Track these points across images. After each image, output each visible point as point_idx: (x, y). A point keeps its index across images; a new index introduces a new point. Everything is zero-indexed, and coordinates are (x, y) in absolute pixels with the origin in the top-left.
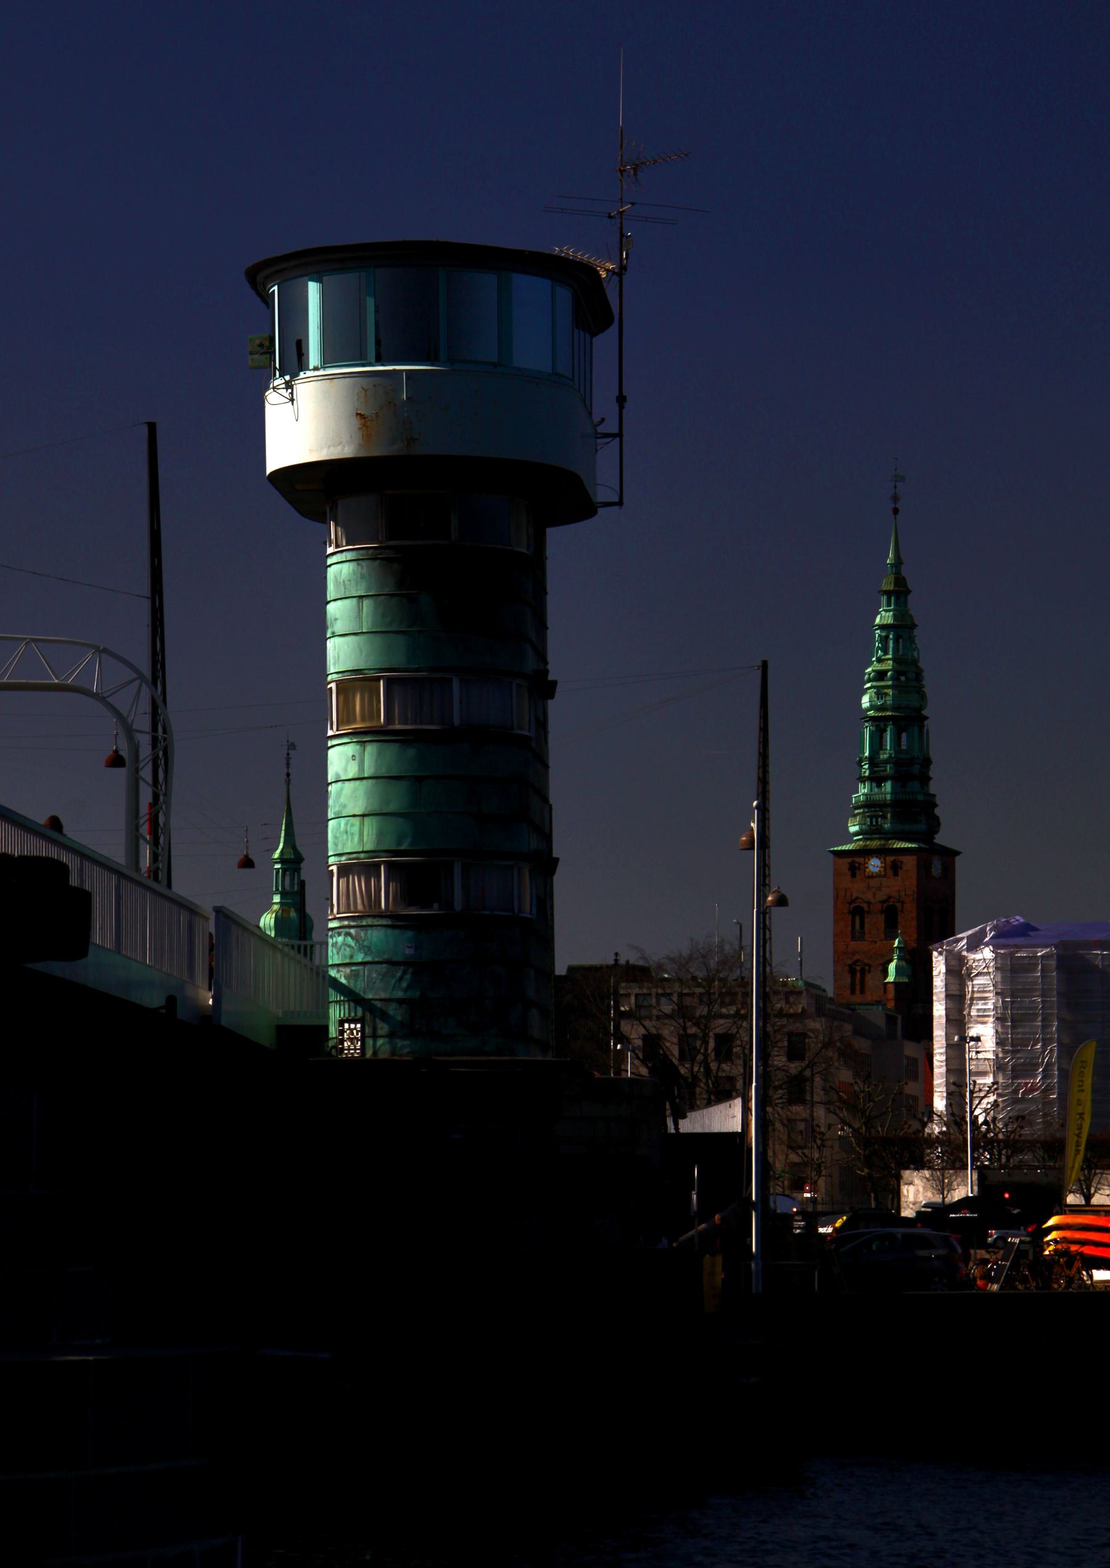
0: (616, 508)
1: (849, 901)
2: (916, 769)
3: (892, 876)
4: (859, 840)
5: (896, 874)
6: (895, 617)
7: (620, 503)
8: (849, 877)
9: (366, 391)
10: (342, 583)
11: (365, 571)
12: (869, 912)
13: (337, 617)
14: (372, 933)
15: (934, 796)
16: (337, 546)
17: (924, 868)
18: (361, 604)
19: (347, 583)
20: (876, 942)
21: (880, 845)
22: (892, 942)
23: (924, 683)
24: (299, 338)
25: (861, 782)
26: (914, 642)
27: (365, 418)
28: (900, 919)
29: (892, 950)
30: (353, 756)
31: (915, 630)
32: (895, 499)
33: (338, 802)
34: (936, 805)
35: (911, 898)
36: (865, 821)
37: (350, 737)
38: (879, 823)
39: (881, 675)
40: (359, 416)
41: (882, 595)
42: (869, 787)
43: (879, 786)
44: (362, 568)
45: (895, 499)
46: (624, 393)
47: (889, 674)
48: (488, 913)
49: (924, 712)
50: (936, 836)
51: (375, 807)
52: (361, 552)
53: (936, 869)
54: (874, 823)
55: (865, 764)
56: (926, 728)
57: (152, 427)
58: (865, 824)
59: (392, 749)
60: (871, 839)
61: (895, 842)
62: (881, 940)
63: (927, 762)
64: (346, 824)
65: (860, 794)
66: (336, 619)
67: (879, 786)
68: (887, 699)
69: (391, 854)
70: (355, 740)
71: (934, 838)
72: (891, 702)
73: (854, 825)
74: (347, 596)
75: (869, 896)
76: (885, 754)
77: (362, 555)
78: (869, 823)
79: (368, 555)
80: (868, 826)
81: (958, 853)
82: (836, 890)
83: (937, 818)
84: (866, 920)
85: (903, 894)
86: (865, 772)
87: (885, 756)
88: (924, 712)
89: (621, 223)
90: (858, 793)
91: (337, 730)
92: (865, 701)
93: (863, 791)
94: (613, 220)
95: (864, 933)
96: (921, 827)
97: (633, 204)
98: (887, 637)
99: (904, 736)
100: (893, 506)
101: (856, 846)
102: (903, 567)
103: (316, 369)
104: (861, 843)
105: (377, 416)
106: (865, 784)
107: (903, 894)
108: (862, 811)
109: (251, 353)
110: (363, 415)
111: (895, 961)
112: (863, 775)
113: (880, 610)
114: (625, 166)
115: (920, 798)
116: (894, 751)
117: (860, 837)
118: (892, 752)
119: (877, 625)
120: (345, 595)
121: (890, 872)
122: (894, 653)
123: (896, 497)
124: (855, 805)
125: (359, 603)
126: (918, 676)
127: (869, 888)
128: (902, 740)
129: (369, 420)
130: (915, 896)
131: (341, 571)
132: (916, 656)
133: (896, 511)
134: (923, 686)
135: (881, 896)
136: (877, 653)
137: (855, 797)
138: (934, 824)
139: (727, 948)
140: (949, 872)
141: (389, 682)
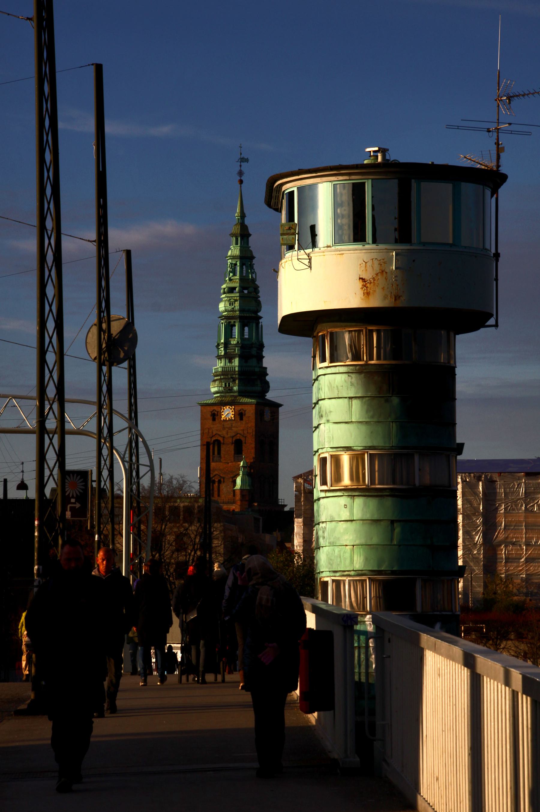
0: (494, 328)
1: (211, 436)
2: (254, 351)
3: (239, 420)
4: (218, 397)
5: (241, 419)
6: (241, 251)
8: (211, 421)
9: (366, 263)
10: (336, 388)
11: (354, 380)
12: (224, 444)
13: (331, 410)
15: (266, 368)
16: (331, 362)
17: (259, 414)
18: (351, 403)
19: (340, 388)
20: (228, 463)
21: (231, 400)
22: (239, 463)
23: (259, 294)
24: (313, 224)
25: (219, 359)
26: (253, 267)
27: (365, 282)
28: (244, 448)
29: (239, 469)
30: (345, 505)
31: (254, 260)
32: (241, 173)
33: (333, 536)
34: (267, 375)
35: (252, 434)
36: (222, 384)
37: (343, 492)
38: (231, 386)
39: (231, 290)
40: (361, 280)
41: (233, 237)
42: (224, 362)
43: (230, 362)
44: (352, 378)
45: (241, 173)
46: (499, 251)
47: (237, 289)
48: (438, 613)
49: (260, 314)
50: (267, 394)
51: (363, 541)
52: (351, 367)
53: (267, 416)
54: (227, 386)
55: (222, 347)
56: (260, 324)
58: (221, 386)
59: (373, 503)
60: (225, 397)
61: (241, 398)
62: (231, 462)
63: (261, 346)
64: (340, 551)
65: (218, 367)
66: (331, 412)
67: (230, 362)
68: (235, 305)
69: (374, 573)
70: (346, 494)
71: (266, 396)
72: (238, 307)
73: (214, 387)
74: (340, 397)
75: (224, 433)
76: (234, 340)
78: (224, 386)
79: (356, 370)
80: (223, 388)
81: (281, 405)
82: (202, 429)
84: (222, 449)
85: (246, 432)
86: (221, 353)
87: (235, 342)
88: (260, 314)
89: (498, 136)
90: (217, 366)
91: (331, 486)
92: (222, 307)
93: (220, 365)
94: (491, 133)
95: (220, 457)
96: (258, 388)
97: (510, 124)
98: (236, 264)
99: (246, 329)
100: (240, 178)
101: (215, 400)
102: (246, 218)
104: (219, 398)
105: (374, 280)
106: (221, 360)
107: (246, 432)
108: (219, 377)
109: (282, 234)
110: (364, 279)
111: (241, 475)
112: (220, 354)
113: (231, 247)
114: (502, 97)
115: (257, 369)
116: (240, 339)
117: (218, 395)
118: (239, 340)
119: (229, 256)
120: (338, 396)
121: (238, 418)
122: (240, 276)
123: (241, 172)
124: (215, 374)
125: (349, 402)
126: (256, 289)
128: (245, 331)
129: (368, 283)
130: (254, 433)
131: (335, 380)
132: (254, 277)
133: (241, 182)
134: (259, 297)
135: (231, 434)
136: (229, 275)
137: (215, 369)
138: (266, 387)
139: (175, 482)
141: (371, 456)
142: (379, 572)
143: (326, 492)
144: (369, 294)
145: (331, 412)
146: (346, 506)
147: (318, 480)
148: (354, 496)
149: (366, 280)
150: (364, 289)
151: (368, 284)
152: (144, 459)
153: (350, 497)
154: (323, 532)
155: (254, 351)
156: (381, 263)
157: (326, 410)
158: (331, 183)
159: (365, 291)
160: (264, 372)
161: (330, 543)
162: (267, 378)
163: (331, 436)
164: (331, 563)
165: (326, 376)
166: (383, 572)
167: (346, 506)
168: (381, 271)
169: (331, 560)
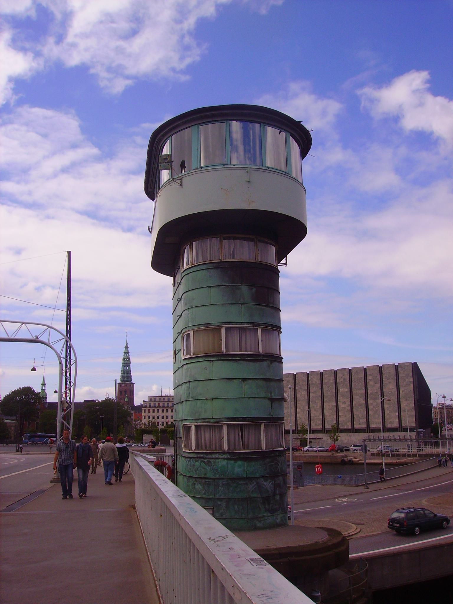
2: (129, 372)
7: (287, 265)
30: (205, 368)
37: (203, 358)
57: (69, 253)
63: (131, 371)
81: (134, 384)
83: (132, 379)
96: (130, 380)
99: (128, 367)
140: (133, 386)
147: (91, 470)
148: (213, 360)
152: (73, 357)
155: (129, 372)
160: (131, 377)
162: (132, 378)
163: (194, 317)
165: (189, 274)
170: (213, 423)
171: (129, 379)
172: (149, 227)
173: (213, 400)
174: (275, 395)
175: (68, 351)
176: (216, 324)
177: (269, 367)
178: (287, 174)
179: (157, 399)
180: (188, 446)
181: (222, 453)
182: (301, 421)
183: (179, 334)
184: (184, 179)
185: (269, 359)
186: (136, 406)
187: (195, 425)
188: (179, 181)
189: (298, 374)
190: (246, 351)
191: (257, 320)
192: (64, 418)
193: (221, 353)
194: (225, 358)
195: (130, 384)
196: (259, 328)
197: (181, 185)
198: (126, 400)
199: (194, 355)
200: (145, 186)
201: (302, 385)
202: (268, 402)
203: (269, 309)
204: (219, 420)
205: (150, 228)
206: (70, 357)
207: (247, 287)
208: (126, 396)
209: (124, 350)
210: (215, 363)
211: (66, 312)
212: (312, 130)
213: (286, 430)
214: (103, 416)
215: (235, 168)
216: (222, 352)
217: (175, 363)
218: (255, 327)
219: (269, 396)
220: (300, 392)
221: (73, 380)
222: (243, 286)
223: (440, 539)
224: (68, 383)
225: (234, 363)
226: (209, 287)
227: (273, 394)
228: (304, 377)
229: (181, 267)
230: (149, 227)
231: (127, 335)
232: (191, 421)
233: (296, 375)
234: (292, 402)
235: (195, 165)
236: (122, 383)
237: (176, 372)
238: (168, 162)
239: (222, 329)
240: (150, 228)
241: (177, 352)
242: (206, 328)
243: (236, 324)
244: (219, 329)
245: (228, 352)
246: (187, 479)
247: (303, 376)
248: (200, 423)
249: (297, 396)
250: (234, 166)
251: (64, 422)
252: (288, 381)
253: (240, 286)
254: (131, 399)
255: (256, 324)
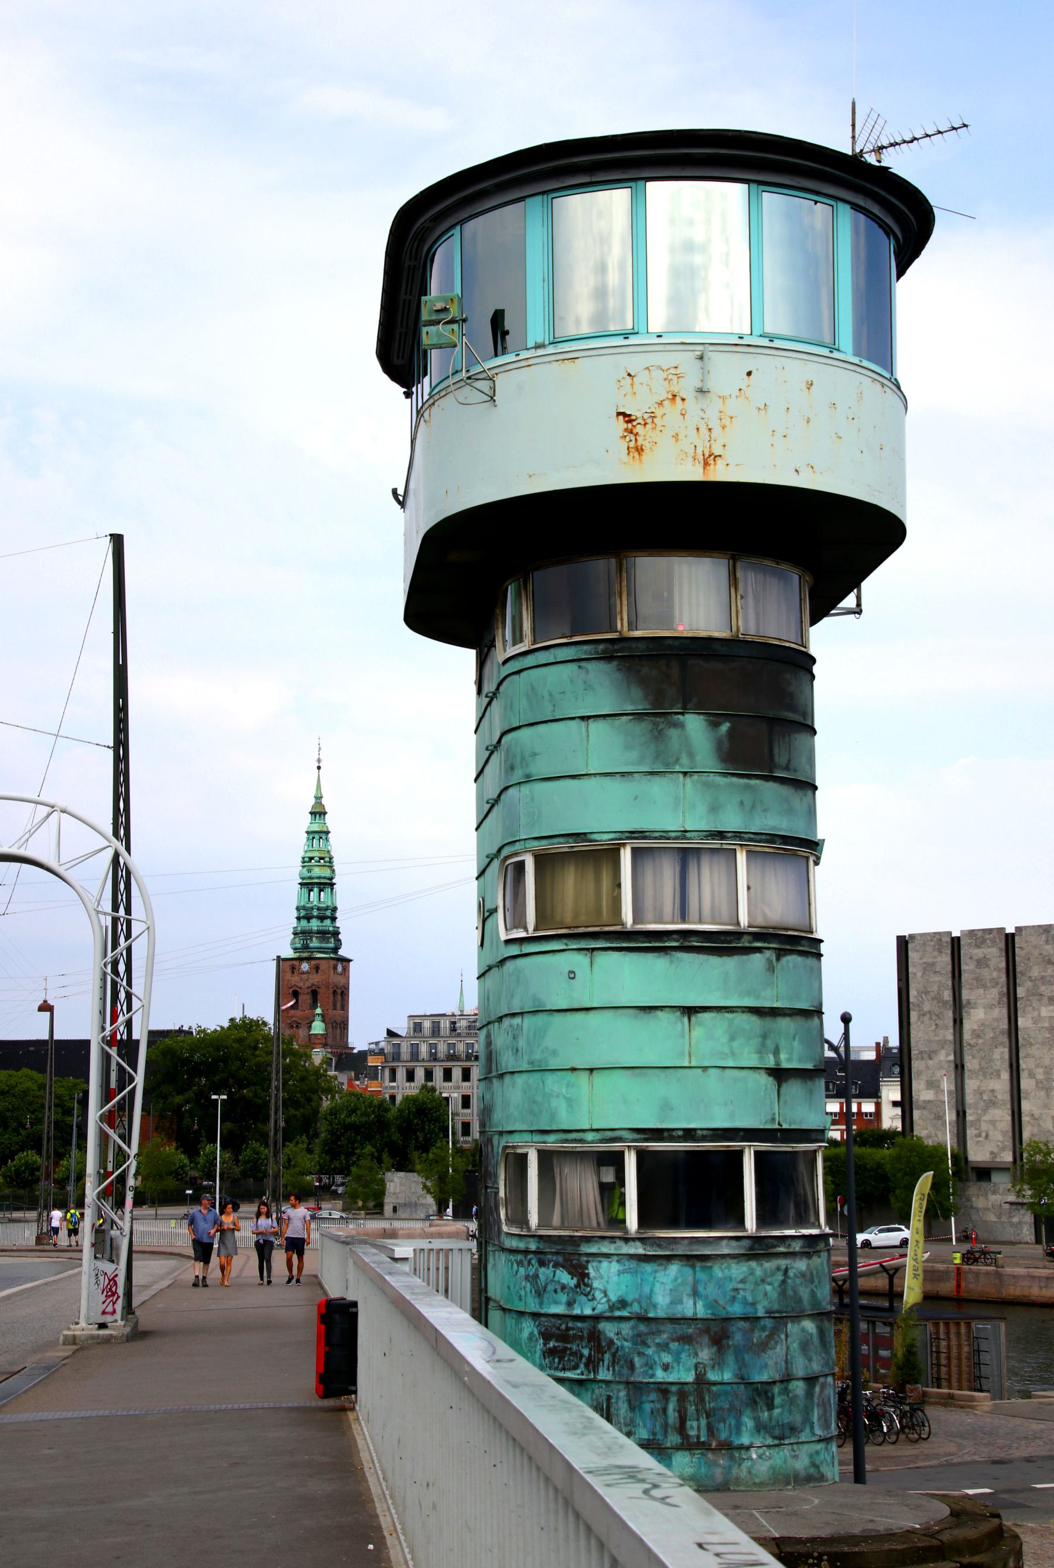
5: (317, 972)
7: (860, 612)
13: (537, 750)
14: (610, 1268)
24: (500, 308)
37: (565, 941)
40: (621, 418)
52: (585, 647)
57: (117, 541)
66: (535, 754)
75: (301, 984)
77: (586, 652)
79: (597, 653)
83: (340, 941)
103: (537, 347)
115: (331, 929)
121: (314, 971)
127: (301, 980)
133: (319, 768)
135: (308, 984)
138: (338, 944)
140: (346, 970)
142: (657, 1134)
143: (521, 944)
144: (642, 450)
145: (535, 754)
146: (572, 976)
148: (594, 949)
149: (633, 418)
150: (628, 439)
151: (639, 426)
153: (582, 952)
154: (514, 1038)
155: (328, 913)
156: (671, 377)
157: (522, 752)
158: (545, 196)
159: (632, 444)
161: (532, 1063)
164: (536, 1109)
165: (523, 674)
166: (666, 1134)
167: (572, 976)
168: (670, 397)
169: (534, 1102)
170: (593, 1143)
171: (328, 942)
172: (395, 492)
173: (595, 1072)
174: (789, 1060)
175: (122, 886)
176: (606, 837)
177: (771, 968)
178: (836, 355)
179: (445, 1024)
180: (520, 1218)
181: (620, 1238)
182: (1036, 1130)
183: (491, 859)
184: (499, 380)
185: (771, 945)
186: (355, 1051)
187: (538, 1148)
188: (484, 385)
189: (1024, 932)
190: (700, 922)
191: (732, 820)
192: (109, 1119)
193: (618, 928)
194: (630, 941)
195: (332, 962)
196: (738, 848)
197: (492, 398)
198: (318, 1027)
199: (536, 929)
200: (382, 331)
201: (1042, 977)
202: (766, 1081)
203: (771, 785)
204: (609, 1134)
205: (401, 491)
206: (128, 911)
207: (702, 717)
208: (319, 1011)
209: (305, 822)
210: (602, 958)
211: (111, 752)
212: (965, 126)
213: (974, 1165)
214: (225, 1097)
215: (661, 348)
216: (623, 925)
217: (482, 945)
218: (726, 844)
219: (771, 1063)
220: (1034, 1009)
221: (137, 989)
222: (687, 716)
223: (143, 1118)
224: (122, 995)
225: (659, 957)
226: (582, 718)
227: (783, 1056)
228: (1048, 947)
229: (499, 643)
230: (395, 492)
231: (319, 761)
232: (527, 1137)
233: (1016, 938)
234: (1000, 1049)
235: (536, 330)
236: (300, 959)
237: (487, 975)
238: (452, 321)
239: (622, 851)
240: (401, 491)
241: (487, 914)
242: (572, 847)
243: (664, 835)
244: (612, 853)
245: (642, 923)
246: (514, 1321)
247: (1047, 942)
248: (551, 1142)
249: (1019, 1023)
250: (660, 341)
251: (111, 1132)
252: (981, 963)
253: (680, 717)
254: (339, 1025)
255: (729, 835)
